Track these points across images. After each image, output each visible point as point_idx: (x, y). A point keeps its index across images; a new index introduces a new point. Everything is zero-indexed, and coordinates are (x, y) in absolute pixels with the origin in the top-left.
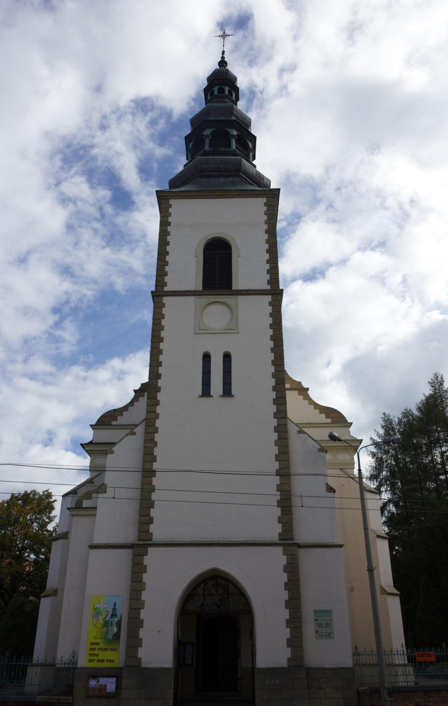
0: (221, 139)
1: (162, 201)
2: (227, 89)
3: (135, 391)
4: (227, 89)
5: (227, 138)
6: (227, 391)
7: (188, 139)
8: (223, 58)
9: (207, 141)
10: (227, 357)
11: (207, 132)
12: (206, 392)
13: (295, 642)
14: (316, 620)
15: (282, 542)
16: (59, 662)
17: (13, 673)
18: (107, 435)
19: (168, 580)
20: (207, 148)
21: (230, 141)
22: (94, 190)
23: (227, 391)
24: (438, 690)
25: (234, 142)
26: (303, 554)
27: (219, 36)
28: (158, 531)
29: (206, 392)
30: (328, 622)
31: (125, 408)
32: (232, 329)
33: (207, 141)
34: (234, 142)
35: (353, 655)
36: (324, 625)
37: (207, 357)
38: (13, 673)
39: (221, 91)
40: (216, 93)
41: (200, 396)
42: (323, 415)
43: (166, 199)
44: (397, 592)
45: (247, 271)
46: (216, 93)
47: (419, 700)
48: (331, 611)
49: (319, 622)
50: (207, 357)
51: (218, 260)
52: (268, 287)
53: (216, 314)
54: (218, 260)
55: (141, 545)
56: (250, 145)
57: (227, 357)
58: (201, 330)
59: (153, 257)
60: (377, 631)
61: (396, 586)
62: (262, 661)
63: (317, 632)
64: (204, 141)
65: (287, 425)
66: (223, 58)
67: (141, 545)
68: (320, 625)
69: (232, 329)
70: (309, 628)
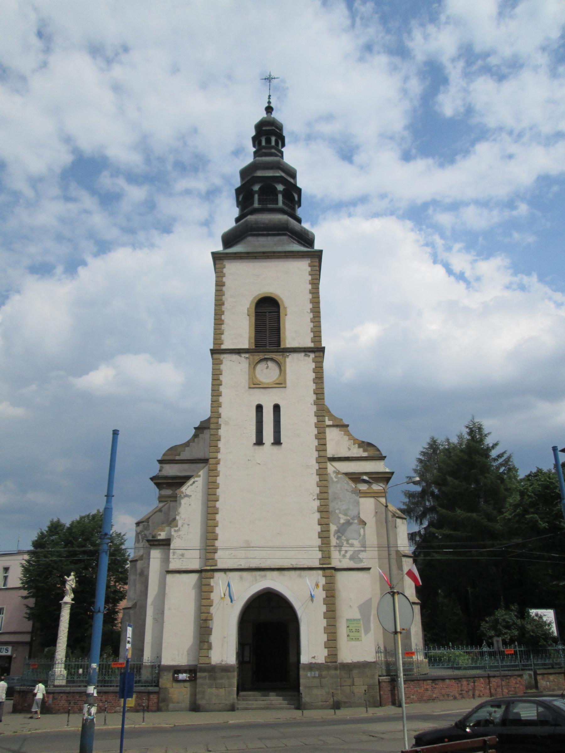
0: (268, 190)
1: (217, 262)
2: (273, 139)
3: (195, 428)
4: (273, 139)
5: (275, 192)
6: (277, 442)
7: (238, 191)
8: (269, 103)
9: (256, 197)
10: (277, 408)
11: (256, 188)
12: (259, 442)
13: (332, 643)
14: (348, 627)
15: (321, 566)
16: (146, 661)
17: (104, 671)
18: (171, 470)
20: (256, 205)
21: (277, 196)
23: (277, 442)
24: (443, 679)
25: (280, 197)
27: (265, 79)
28: (223, 559)
29: (259, 442)
30: (357, 628)
31: (187, 444)
32: (281, 384)
33: (256, 197)
34: (280, 197)
35: (376, 653)
36: (354, 630)
37: (259, 408)
38: (104, 671)
39: (268, 141)
40: (263, 143)
42: (361, 450)
45: (295, 332)
46: (263, 143)
47: (428, 687)
49: (350, 628)
50: (259, 408)
51: (267, 311)
52: (312, 345)
53: (267, 372)
54: (267, 311)
55: (206, 572)
56: (296, 199)
57: (277, 408)
58: (255, 385)
61: (418, 597)
62: (305, 659)
63: (348, 636)
64: (253, 197)
65: (327, 468)
66: (269, 103)
67: (206, 572)
68: (351, 631)
69: (281, 384)
70: (342, 631)
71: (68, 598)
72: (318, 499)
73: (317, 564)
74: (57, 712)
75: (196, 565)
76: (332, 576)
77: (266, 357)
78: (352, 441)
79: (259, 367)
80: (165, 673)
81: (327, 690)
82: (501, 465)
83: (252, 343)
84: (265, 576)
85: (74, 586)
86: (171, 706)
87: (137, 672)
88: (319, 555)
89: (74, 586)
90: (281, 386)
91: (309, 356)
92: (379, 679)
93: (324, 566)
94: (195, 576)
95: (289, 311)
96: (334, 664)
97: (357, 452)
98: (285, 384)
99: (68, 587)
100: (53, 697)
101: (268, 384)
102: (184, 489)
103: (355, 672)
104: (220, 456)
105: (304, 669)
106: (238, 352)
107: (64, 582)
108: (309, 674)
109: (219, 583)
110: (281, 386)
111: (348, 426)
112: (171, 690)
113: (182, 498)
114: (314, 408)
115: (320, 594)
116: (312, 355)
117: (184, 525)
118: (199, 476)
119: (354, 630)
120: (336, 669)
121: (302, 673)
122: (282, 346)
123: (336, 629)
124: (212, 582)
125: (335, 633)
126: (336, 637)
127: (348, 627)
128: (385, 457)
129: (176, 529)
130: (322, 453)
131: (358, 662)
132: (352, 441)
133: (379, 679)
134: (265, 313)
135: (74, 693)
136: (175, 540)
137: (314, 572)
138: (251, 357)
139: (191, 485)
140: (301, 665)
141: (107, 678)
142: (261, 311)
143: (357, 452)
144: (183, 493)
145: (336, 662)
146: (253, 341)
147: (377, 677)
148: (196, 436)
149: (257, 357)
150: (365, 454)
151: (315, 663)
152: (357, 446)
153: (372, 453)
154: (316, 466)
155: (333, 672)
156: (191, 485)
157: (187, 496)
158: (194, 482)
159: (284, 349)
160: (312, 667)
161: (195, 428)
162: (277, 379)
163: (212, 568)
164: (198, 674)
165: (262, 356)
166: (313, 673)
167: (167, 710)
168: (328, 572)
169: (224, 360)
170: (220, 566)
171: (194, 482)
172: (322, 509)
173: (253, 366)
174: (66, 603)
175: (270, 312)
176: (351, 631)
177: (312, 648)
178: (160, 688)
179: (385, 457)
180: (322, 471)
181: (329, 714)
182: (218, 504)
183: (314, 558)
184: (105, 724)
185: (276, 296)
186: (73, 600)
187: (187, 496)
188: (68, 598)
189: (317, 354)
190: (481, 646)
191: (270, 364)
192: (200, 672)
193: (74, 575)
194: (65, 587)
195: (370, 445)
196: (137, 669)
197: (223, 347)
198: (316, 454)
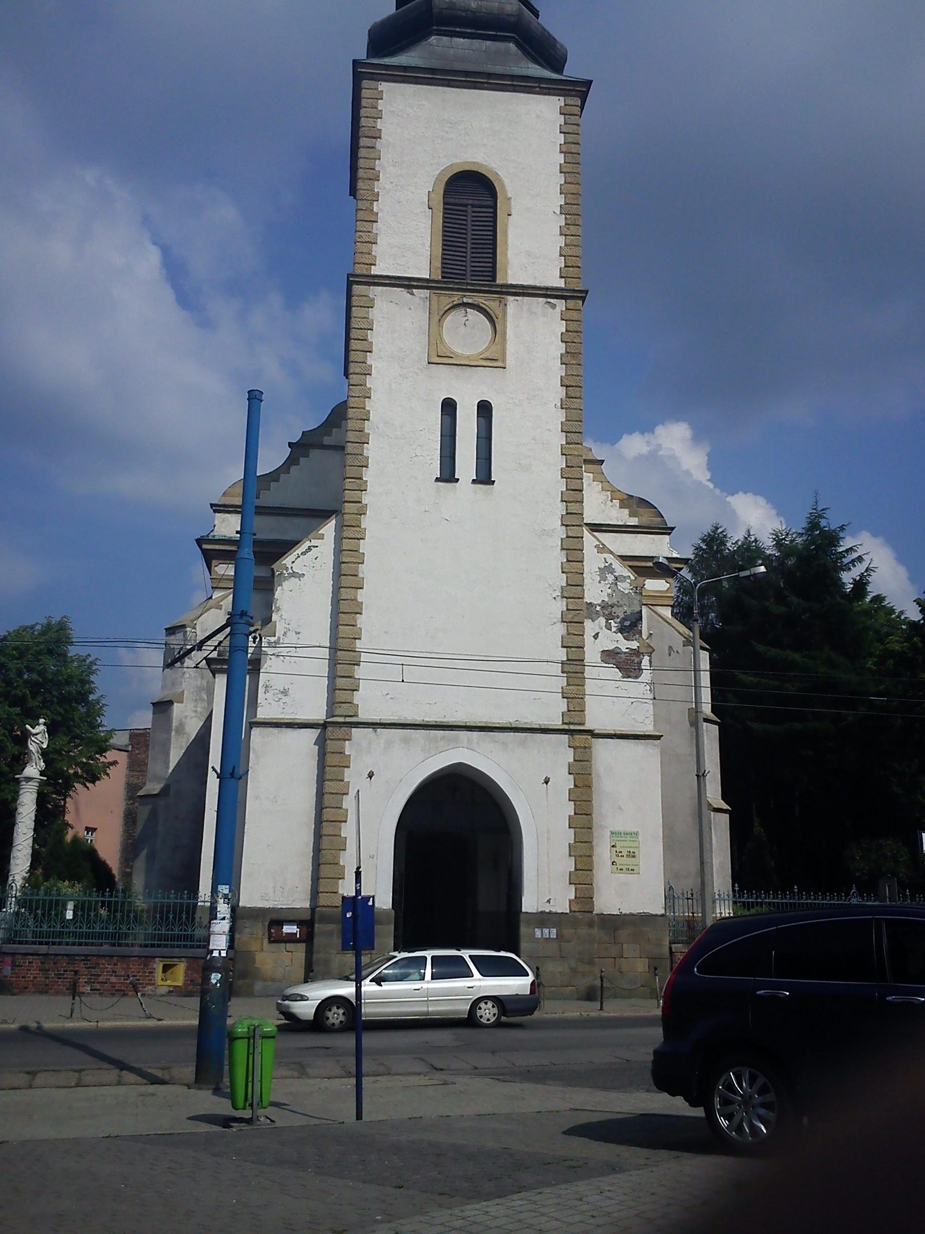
6: (484, 477)
10: (485, 409)
12: (448, 475)
14: (613, 846)
15: (566, 727)
19: (384, 784)
22: (642, 1011)
23: (484, 477)
26: (601, 748)
28: (370, 702)
29: (448, 475)
32: (494, 361)
37: (449, 407)
41: (437, 480)
42: (626, 511)
43: (373, 79)
44: (726, 807)
48: (354, 61)
50: (449, 407)
52: (561, 284)
53: (466, 332)
55: (334, 729)
57: (485, 409)
58: (440, 358)
59: (382, 291)
60: (703, 884)
62: (530, 903)
67: (334, 729)
69: (494, 361)
70: (603, 853)
71: (33, 770)
72: (563, 597)
73: (557, 723)
74: (24, 990)
75: (319, 713)
76: (587, 748)
77: (465, 300)
78: (609, 493)
79: (449, 318)
80: (248, 924)
81: (573, 965)
82: (103, 731)
83: (437, 269)
84: (456, 740)
85: (45, 746)
86: (258, 986)
87: (187, 918)
88: (563, 705)
89: (45, 746)
90: (495, 364)
91: (554, 306)
92: (670, 948)
93: (572, 727)
94: (313, 734)
95: (516, 206)
96: (588, 915)
97: (622, 517)
98: (504, 361)
99: (33, 747)
100: (13, 962)
101: (468, 357)
102: (287, 560)
103: (623, 934)
104: (366, 499)
105: (529, 923)
106: (408, 284)
107: (26, 736)
108: (538, 933)
109: (363, 750)
110: (495, 364)
111: (602, 461)
112: (259, 957)
113: (286, 579)
114: (561, 416)
115: (564, 782)
116: (561, 305)
117: (289, 634)
118: (322, 537)
119: (625, 853)
120: (590, 925)
121: (523, 930)
122: (499, 281)
123: (591, 848)
124: (348, 748)
125: (590, 856)
126: (591, 863)
127: (613, 846)
128: (673, 529)
129: (273, 639)
130: (573, 508)
131: (621, 916)
132: (609, 493)
133: (670, 948)
134: (466, 205)
135: (56, 955)
136: (269, 662)
137: (610, 728)
138: (434, 298)
139: (303, 553)
140: (522, 917)
141: (124, 929)
142: (457, 201)
143: (622, 517)
144: (287, 569)
145: (592, 912)
146: (438, 264)
147: (666, 943)
148: (291, 461)
149: (447, 299)
150: (634, 521)
151: (550, 913)
152: (617, 502)
153: (646, 518)
154: (562, 532)
155: (583, 931)
156: (303, 553)
157: (294, 575)
158: (309, 549)
159: (502, 286)
160: (544, 919)
161: (290, 445)
162: (486, 350)
163: (348, 720)
164: (316, 925)
165: (456, 298)
166: (546, 931)
167: (250, 994)
168: (579, 739)
169: (378, 303)
170: (363, 716)
171: (309, 549)
172: (569, 617)
173: (438, 318)
174: (29, 779)
175: (473, 206)
176: (619, 854)
177: (544, 886)
178: (236, 952)
179: (673, 529)
180: (572, 543)
181: (591, 1010)
182: (361, 596)
183: (552, 711)
184: (601, 1009)
185: (490, 171)
186: (42, 773)
187: (294, 575)
188: (33, 770)
189: (571, 303)
190: (847, 894)
191: (473, 314)
192: (320, 922)
193: (45, 724)
194: (27, 747)
195: (643, 503)
196: (174, 913)
197: (375, 271)
198: (561, 509)
